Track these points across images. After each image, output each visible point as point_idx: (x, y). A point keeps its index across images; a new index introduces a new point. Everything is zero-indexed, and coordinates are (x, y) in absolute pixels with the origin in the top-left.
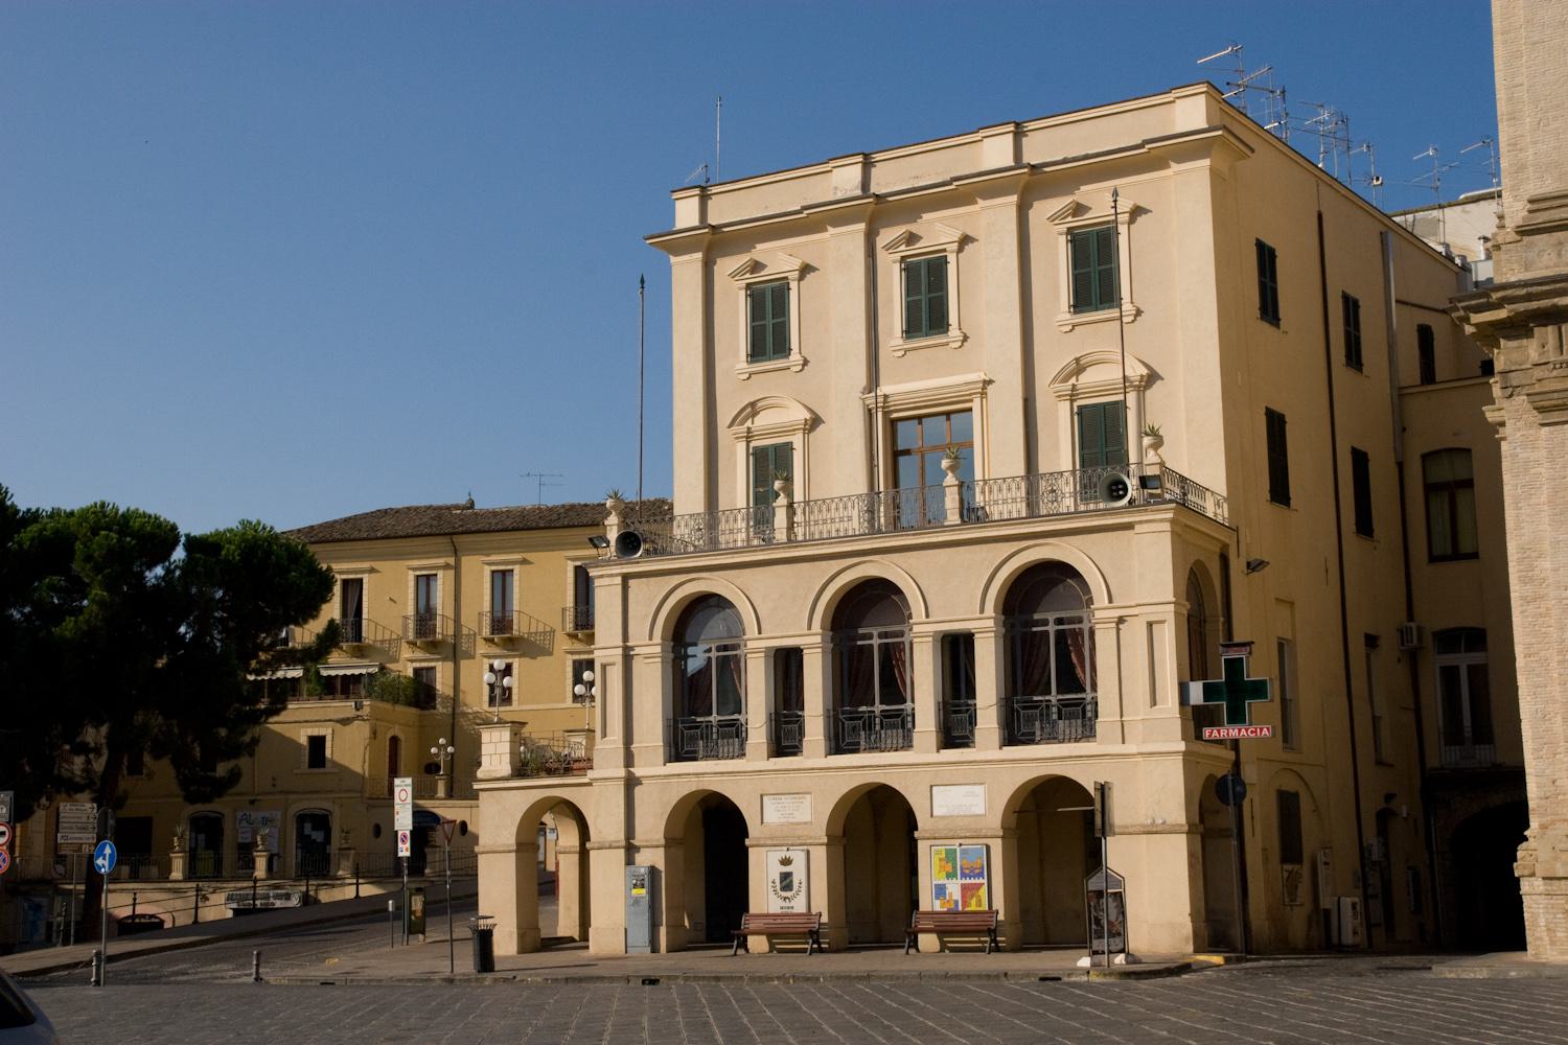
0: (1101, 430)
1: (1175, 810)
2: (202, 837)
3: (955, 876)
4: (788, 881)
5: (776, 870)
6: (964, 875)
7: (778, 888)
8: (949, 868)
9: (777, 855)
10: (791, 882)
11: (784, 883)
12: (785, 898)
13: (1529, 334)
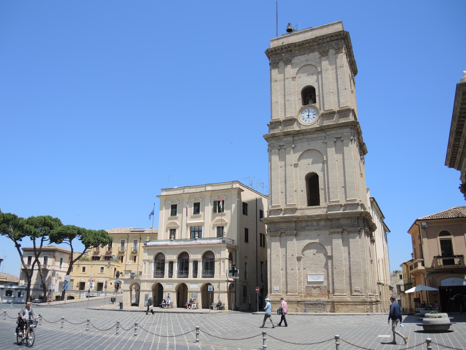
5: (167, 295)
9: (167, 293)
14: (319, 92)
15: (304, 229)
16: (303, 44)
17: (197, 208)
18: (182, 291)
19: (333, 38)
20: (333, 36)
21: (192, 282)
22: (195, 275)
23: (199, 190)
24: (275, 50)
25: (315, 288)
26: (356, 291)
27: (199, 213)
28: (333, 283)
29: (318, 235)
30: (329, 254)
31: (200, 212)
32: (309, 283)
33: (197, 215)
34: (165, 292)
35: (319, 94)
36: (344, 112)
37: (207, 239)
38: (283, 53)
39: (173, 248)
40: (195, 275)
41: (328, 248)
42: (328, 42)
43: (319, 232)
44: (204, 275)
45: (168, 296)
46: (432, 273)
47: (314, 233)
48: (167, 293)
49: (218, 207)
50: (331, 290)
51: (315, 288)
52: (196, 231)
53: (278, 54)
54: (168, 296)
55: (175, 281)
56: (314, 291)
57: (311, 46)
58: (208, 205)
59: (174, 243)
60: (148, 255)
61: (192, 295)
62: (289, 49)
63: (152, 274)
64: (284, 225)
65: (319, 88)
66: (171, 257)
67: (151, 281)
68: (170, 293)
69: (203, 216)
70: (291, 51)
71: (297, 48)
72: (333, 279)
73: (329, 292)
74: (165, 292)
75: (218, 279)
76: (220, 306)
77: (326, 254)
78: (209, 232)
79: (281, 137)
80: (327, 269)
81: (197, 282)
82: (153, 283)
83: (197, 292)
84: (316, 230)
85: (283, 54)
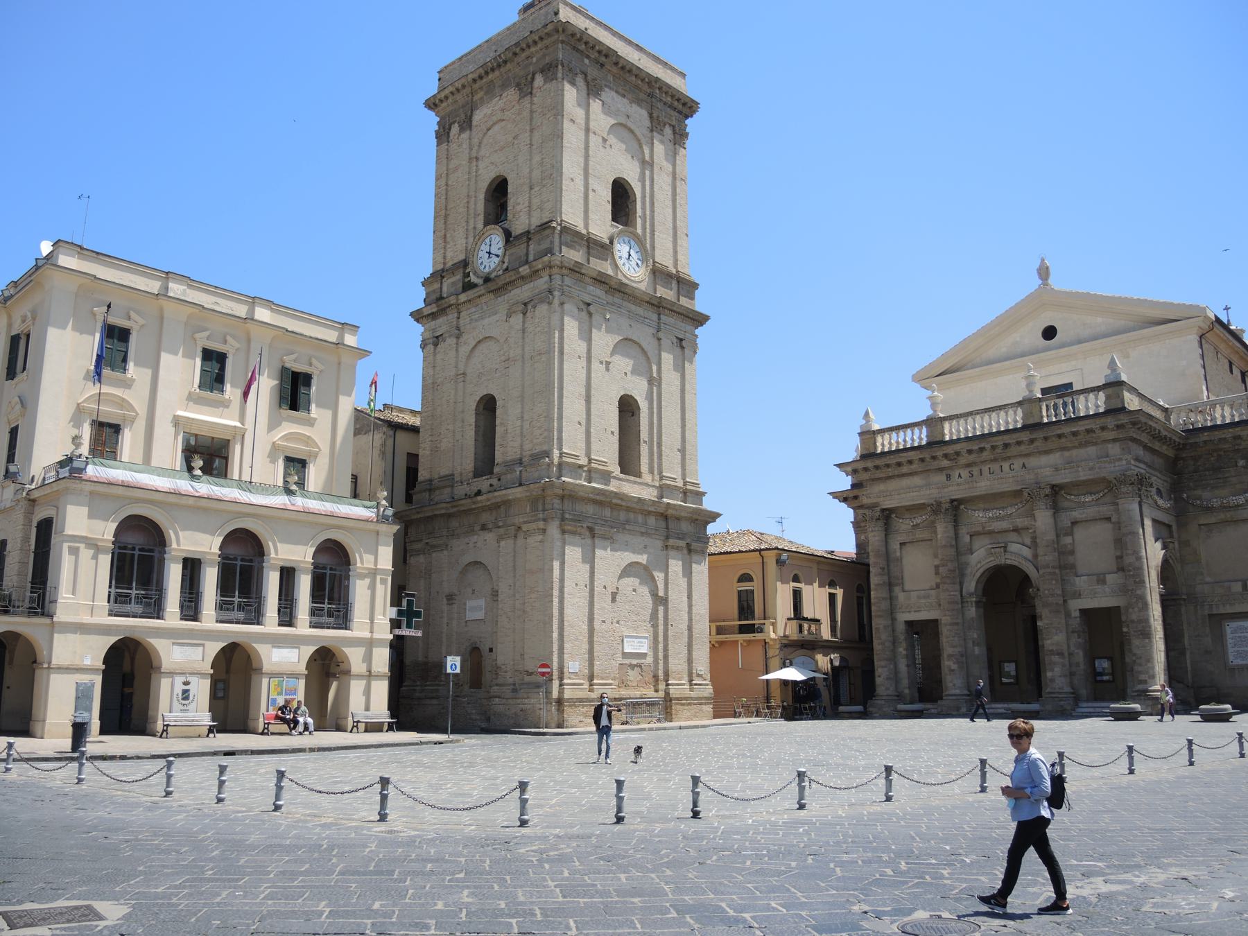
5: (179, 688)
9: (179, 680)
14: (644, 209)
15: (622, 526)
16: (630, 71)
17: (215, 368)
18: (233, 675)
19: (676, 103)
20: (678, 100)
21: (277, 641)
23: (225, 306)
24: (580, 40)
25: (632, 667)
26: (699, 676)
27: (125, 370)
28: (666, 657)
29: (645, 547)
30: (661, 593)
32: (625, 655)
33: (215, 395)
34: (171, 674)
35: (644, 215)
37: (248, 486)
38: (588, 57)
39: (205, 510)
41: (659, 576)
42: (665, 104)
43: (646, 540)
44: (315, 619)
45: (185, 692)
46: (786, 646)
47: (639, 541)
48: (179, 680)
49: (294, 391)
50: (661, 674)
51: (632, 667)
52: (208, 455)
53: (578, 50)
55: (210, 635)
56: (633, 675)
57: (637, 87)
58: (64, 327)
59: (300, 502)
61: (280, 685)
62: (603, 59)
64: (590, 509)
65: (644, 197)
66: (291, 552)
68: (190, 679)
70: (602, 65)
71: (614, 70)
72: (666, 649)
73: (656, 677)
74: (171, 674)
77: (654, 594)
78: (256, 463)
79: (589, 280)
80: (655, 626)
82: (113, 640)
83: (295, 676)
84: (642, 534)
85: (587, 61)
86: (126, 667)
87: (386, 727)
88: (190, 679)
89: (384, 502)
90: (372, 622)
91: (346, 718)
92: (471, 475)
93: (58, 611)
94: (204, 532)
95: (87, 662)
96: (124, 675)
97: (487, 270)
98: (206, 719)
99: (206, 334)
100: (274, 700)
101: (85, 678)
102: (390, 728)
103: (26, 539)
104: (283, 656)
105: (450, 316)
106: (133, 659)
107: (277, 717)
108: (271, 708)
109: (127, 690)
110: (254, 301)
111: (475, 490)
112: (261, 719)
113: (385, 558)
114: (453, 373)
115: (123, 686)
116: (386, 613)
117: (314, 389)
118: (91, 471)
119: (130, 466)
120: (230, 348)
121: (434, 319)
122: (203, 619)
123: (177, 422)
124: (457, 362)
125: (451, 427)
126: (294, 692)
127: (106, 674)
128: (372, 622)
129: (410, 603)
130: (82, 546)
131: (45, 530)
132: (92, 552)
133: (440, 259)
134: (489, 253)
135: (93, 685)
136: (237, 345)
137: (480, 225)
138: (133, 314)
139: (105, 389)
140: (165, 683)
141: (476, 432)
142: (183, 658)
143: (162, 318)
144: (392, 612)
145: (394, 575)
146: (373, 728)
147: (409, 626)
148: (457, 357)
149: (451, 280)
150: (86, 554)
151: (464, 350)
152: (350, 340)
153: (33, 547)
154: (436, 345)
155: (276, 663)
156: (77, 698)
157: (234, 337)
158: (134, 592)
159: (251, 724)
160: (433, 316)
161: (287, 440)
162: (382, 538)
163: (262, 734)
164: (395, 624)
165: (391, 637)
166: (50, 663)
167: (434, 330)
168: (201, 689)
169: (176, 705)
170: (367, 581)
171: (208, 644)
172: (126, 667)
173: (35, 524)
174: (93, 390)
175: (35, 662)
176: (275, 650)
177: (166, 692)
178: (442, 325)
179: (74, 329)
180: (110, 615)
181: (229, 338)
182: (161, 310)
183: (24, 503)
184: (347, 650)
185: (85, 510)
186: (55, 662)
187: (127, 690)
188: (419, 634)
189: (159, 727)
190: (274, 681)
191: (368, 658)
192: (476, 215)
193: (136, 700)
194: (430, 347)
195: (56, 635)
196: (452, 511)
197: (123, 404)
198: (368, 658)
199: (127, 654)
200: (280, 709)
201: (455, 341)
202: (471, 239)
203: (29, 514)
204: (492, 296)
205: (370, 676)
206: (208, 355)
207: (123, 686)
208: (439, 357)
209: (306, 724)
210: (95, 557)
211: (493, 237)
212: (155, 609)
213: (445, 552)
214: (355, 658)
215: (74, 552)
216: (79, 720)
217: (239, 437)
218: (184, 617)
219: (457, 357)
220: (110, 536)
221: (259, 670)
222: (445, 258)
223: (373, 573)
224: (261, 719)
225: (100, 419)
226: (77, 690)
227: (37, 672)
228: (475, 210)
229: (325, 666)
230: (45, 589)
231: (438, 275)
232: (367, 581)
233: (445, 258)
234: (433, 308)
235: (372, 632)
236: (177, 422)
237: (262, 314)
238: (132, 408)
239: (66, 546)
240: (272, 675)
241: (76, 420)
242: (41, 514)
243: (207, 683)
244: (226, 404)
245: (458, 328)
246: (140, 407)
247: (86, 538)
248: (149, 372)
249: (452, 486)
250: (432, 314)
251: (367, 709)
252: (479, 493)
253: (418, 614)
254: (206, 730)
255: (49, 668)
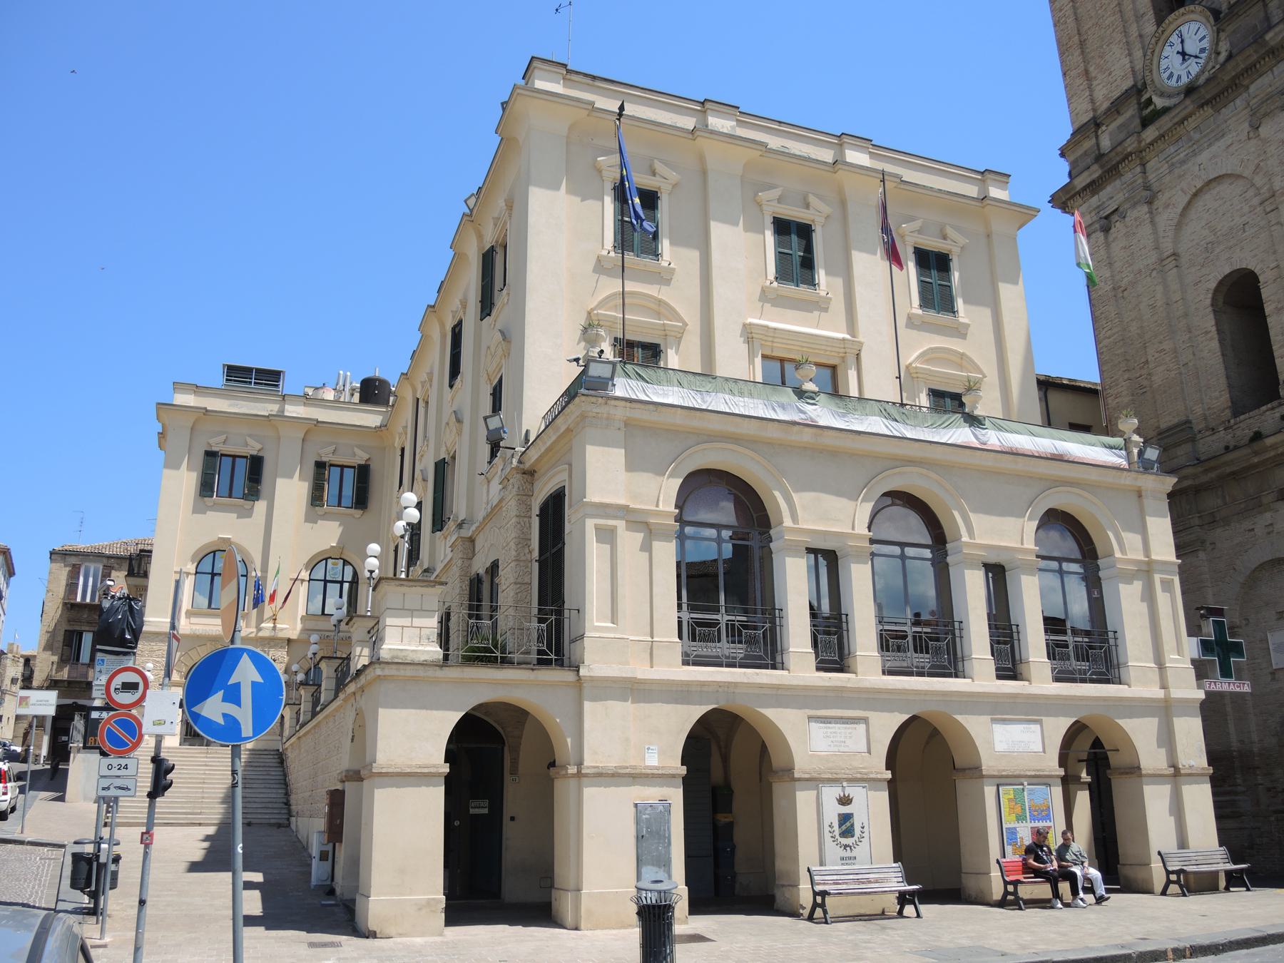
0: (937, 297)
1: (433, 755)
2: (318, 870)
3: (1024, 819)
4: (848, 824)
5: (832, 811)
6: (1033, 819)
7: (837, 833)
8: (1018, 809)
9: (830, 794)
10: (852, 825)
11: (844, 827)
12: (846, 846)
13: (676, 507)
17: (797, 249)
18: (926, 770)
22: (1010, 667)
31: (821, 276)
34: (815, 782)
36: (571, 128)
40: (1010, 667)
45: (845, 819)
48: (830, 794)
54: (845, 819)
55: (876, 700)
60: (631, 466)
61: (1017, 799)
63: (667, 632)
67: (678, 693)
68: (852, 791)
69: (838, 304)
74: (815, 782)
75: (1153, 692)
76: (150, 735)
81: (1031, 710)
83: (1040, 779)
86: (717, 775)
87: (1222, 883)
88: (852, 791)
89: (1136, 438)
90: (1161, 666)
91: (1146, 864)
92: (1228, 413)
93: (588, 657)
94: (839, 493)
95: (652, 761)
96: (714, 790)
97: (1185, 80)
98: (893, 880)
99: (775, 193)
100: (1013, 832)
101: (650, 794)
102: (1234, 880)
103: (524, 541)
104: (1015, 741)
105: (1128, 176)
106: (725, 759)
107: (1027, 869)
108: (1009, 849)
109: (723, 818)
110: (841, 140)
111: (1249, 433)
112: (995, 873)
113: (1160, 538)
114: (1153, 257)
115: (715, 810)
116: (1182, 652)
117: (956, 276)
118: (623, 387)
119: (684, 377)
120: (815, 214)
121: (1094, 193)
122: (860, 669)
123: (750, 334)
124: (1156, 240)
125: (1167, 345)
126: (1046, 814)
127: (691, 786)
128: (1161, 666)
129: (1219, 626)
130: (620, 524)
131: (553, 515)
132: (639, 537)
133: (1086, 106)
134: (1183, 54)
135: (668, 809)
136: (826, 209)
137: (1150, 27)
138: (658, 166)
139: (631, 286)
140: (804, 800)
141: (1221, 341)
142: (832, 744)
143: (704, 173)
144: (1192, 647)
145: (1183, 572)
146: (1194, 884)
147: (1226, 673)
148: (1155, 232)
149: (1114, 125)
150: (629, 540)
151: (1166, 218)
152: (995, 192)
153: (536, 554)
154: (1106, 230)
155: (1003, 755)
156: (640, 838)
157: (820, 198)
158: (723, 618)
159: (970, 884)
160: (1094, 187)
161: (927, 361)
162: (1148, 503)
163: (1002, 904)
164: (1201, 670)
165: (1201, 695)
166: (580, 764)
167: (1099, 208)
168: (873, 810)
169: (833, 851)
170: (1138, 586)
171: (874, 716)
172: (717, 775)
173: (536, 511)
174: (612, 286)
175: (552, 764)
176: (998, 728)
177: (808, 818)
178: (1113, 194)
179: (569, 191)
180: (686, 663)
181: (812, 199)
182: (702, 159)
183: (516, 479)
184: (1127, 724)
185: (618, 455)
186: (590, 761)
187: (723, 818)
188: (1246, 688)
189: (805, 896)
190: (1007, 792)
191: (1167, 739)
192: (1139, 17)
193: (742, 836)
194: (1100, 236)
195: (587, 705)
196: (1204, 479)
197: (660, 308)
198: (1167, 739)
199: (714, 749)
200: (1029, 850)
201: (1145, 208)
202: (1138, 54)
203: (525, 496)
204: (1208, 110)
205: (1176, 775)
206: (782, 227)
207: (715, 810)
208: (1116, 248)
209: (1087, 879)
210: (647, 547)
211: (1184, 29)
212: (768, 651)
213: (1202, 555)
214: (1142, 737)
215: (607, 535)
216: (651, 898)
217: (851, 359)
218: (823, 666)
219: (1155, 232)
220: (668, 505)
221: (975, 771)
222: (1092, 101)
223: (1146, 570)
224: (995, 873)
225: (628, 337)
226: (638, 821)
227: (558, 784)
228: (1135, 10)
229: (1094, 763)
230: (560, 612)
231: (1087, 129)
232: (1138, 586)
233: (1092, 101)
234: (1096, 172)
235: (1164, 686)
236: (750, 334)
237: (856, 157)
238: (676, 315)
239: (590, 524)
240: (1002, 780)
241: (589, 331)
242: (543, 491)
243: (882, 799)
244: (821, 306)
245: (1147, 187)
246: (690, 314)
247: (625, 509)
248: (695, 255)
249: (1193, 440)
250: (1093, 182)
251: (1183, 844)
252: (1258, 436)
253: (1237, 649)
254: (892, 904)
255: (579, 774)
